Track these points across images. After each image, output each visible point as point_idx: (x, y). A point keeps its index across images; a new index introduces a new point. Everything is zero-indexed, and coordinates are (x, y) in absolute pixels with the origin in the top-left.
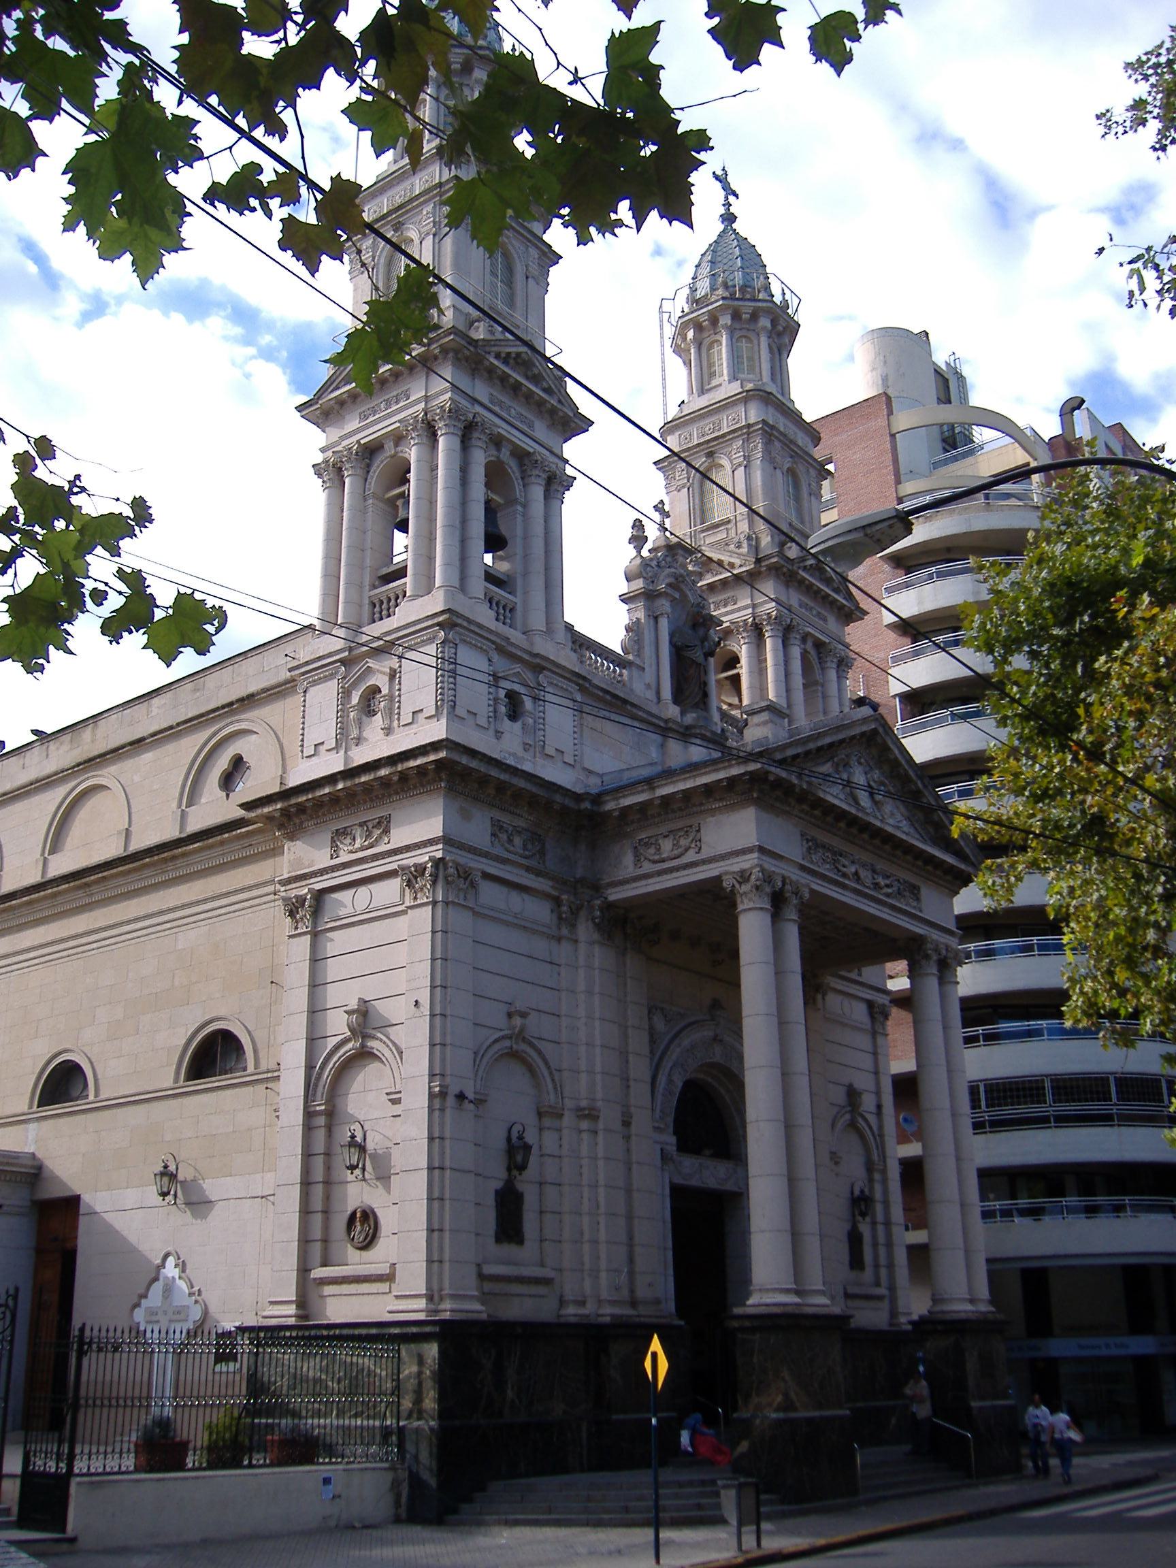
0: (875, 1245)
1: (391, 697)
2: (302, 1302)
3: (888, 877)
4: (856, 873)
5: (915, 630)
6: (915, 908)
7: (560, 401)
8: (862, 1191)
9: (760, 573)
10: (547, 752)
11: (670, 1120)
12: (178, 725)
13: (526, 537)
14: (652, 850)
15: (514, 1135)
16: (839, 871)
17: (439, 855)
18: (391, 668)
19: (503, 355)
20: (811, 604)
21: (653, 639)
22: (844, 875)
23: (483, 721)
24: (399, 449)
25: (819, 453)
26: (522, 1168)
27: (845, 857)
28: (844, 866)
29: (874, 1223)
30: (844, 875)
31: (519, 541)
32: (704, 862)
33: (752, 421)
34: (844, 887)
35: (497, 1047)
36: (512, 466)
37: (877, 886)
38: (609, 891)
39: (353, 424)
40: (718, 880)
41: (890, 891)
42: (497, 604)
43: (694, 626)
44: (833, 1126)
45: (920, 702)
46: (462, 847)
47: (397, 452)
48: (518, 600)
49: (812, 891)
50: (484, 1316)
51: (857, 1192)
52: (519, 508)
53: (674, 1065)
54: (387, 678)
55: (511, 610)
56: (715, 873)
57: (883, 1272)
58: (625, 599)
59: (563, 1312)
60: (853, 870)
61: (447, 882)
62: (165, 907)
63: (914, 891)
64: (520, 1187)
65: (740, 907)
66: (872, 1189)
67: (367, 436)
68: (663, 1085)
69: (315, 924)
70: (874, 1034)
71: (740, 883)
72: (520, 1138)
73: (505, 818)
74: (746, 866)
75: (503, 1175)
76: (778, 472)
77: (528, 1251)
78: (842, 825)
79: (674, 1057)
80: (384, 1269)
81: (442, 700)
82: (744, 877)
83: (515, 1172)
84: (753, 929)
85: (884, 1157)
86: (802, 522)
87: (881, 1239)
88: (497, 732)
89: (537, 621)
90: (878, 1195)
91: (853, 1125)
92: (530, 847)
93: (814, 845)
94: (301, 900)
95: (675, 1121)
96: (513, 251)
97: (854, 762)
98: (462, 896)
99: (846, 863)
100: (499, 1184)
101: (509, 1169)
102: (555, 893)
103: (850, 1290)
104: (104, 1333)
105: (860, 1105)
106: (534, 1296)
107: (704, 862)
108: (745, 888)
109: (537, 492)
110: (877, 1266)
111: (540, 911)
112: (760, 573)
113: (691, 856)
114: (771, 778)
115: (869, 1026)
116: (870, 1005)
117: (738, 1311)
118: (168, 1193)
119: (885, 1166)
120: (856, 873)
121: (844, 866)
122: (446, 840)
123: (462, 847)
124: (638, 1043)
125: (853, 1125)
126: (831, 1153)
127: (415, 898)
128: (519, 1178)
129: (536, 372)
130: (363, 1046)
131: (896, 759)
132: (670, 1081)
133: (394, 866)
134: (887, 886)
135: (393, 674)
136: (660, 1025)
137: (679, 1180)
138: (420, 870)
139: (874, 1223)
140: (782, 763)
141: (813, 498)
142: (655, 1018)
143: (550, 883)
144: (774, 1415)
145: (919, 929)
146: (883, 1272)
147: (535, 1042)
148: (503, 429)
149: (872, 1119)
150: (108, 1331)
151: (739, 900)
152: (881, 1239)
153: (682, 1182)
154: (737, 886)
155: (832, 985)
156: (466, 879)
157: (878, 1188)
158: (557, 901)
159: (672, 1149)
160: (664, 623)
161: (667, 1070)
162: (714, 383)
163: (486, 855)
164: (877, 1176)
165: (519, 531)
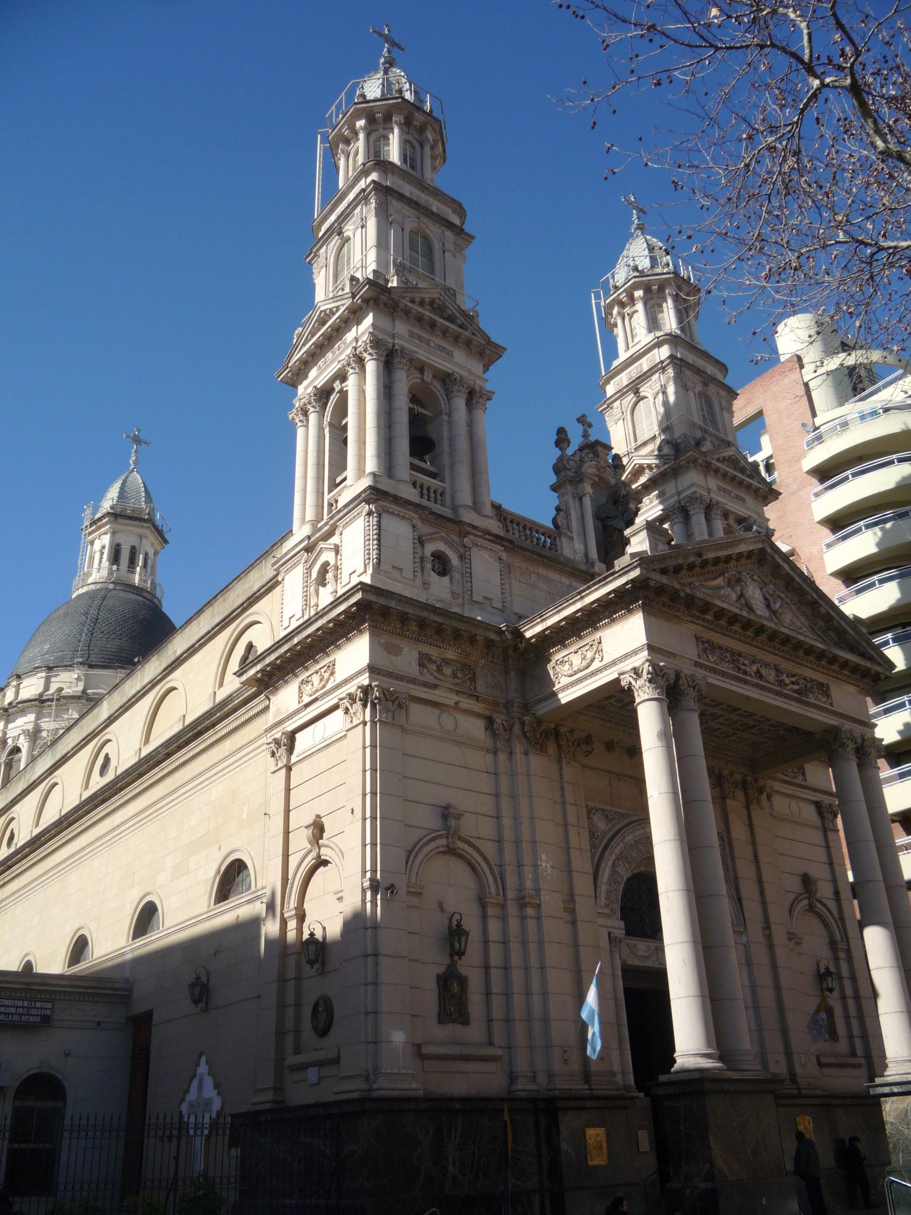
0: (847, 1017)
1: (337, 568)
2: (279, 1089)
3: (793, 676)
4: (758, 671)
5: (839, 523)
6: (825, 702)
7: (473, 334)
8: (827, 969)
9: (681, 467)
10: (474, 598)
11: (617, 906)
12: (213, 629)
13: (451, 440)
14: (567, 667)
15: (455, 923)
16: (739, 669)
17: (366, 682)
18: (335, 545)
19: (417, 300)
20: (728, 487)
21: (579, 513)
22: (745, 673)
23: (409, 574)
24: (343, 385)
25: (728, 381)
26: (461, 954)
27: (745, 658)
28: (744, 665)
29: (843, 998)
30: (745, 673)
31: (446, 442)
32: (606, 667)
33: (662, 359)
34: (746, 682)
35: (433, 845)
36: (437, 386)
37: (781, 683)
38: (537, 708)
39: (313, 373)
40: (617, 681)
41: (796, 687)
42: (435, 492)
43: (616, 502)
44: (791, 910)
45: (852, 575)
46: (390, 675)
47: (342, 388)
48: (447, 485)
49: (710, 685)
50: (421, 1093)
51: (822, 970)
52: (445, 417)
53: (618, 859)
54: (333, 554)
55: (442, 494)
56: (615, 676)
57: (858, 1042)
58: (554, 488)
59: (514, 1088)
60: (755, 668)
61: (374, 706)
62: (203, 769)
63: (824, 689)
64: (463, 971)
65: (638, 700)
66: (837, 966)
67: (319, 383)
68: (606, 876)
69: (289, 759)
70: (825, 830)
71: (636, 680)
72: (459, 925)
73: (433, 652)
74: (637, 664)
75: (446, 961)
76: (691, 394)
77: (475, 1032)
78: (737, 627)
79: (617, 851)
80: (333, 1054)
81: (369, 559)
82: (637, 672)
83: (456, 958)
84: (649, 719)
85: (847, 938)
86: (718, 430)
87: (852, 1011)
88: (424, 583)
89: (465, 498)
90: (845, 972)
91: (811, 908)
92: (460, 675)
93: (708, 647)
94: (277, 742)
95: (622, 908)
96: (430, 234)
97: (746, 577)
98: (390, 716)
99: (746, 662)
100: (441, 970)
101: (451, 956)
102: (488, 713)
103: (823, 1060)
104: (84, 1121)
105: (816, 891)
106: (803, 1105)
107: (606, 667)
108: (640, 682)
109: (460, 403)
110: (851, 1037)
111: (476, 728)
112: (681, 467)
113: (596, 665)
114: (652, 584)
115: (819, 823)
116: (818, 805)
117: (663, 1078)
118: (200, 1001)
119: (849, 945)
120: (758, 671)
121: (744, 665)
122: (372, 669)
123: (390, 675)
124: (579, 840)
125: (811, 908)
126: (789, 933)
127: (352, 722)
128: (459, 962)
129: (450, 312)
130: (319, 856)
131: (788, 574)
132: (614, 872)
133: (335, 701)
134: (793, 683)
135: (337, 550)
136: (601, 824)
137: (634, 962)
138: (352, 697)
139: (843, 998)
140: (664, 571)
141: (724, 412)
142: (595, 818)
143: (483, 705)
144: (702, 1186)
145: (832, 721)
146: (858, 1042)
147: (474, 841)
148: (422, 354)
149: (832, 905)
150: (88, 1118)
151: (636, 695)
152: (852, 1011)
153: (637, 963)
154: (633, 682)
155: (776, 788)
156: (393, 701)
157: (844, 966)
158: (490, 721)
159: (620, 932)
160: (587, 501)
161: (610, 864)
162: (636, 340)
163: (413, 681)
164: (842, 955)
165: (446, 435)
